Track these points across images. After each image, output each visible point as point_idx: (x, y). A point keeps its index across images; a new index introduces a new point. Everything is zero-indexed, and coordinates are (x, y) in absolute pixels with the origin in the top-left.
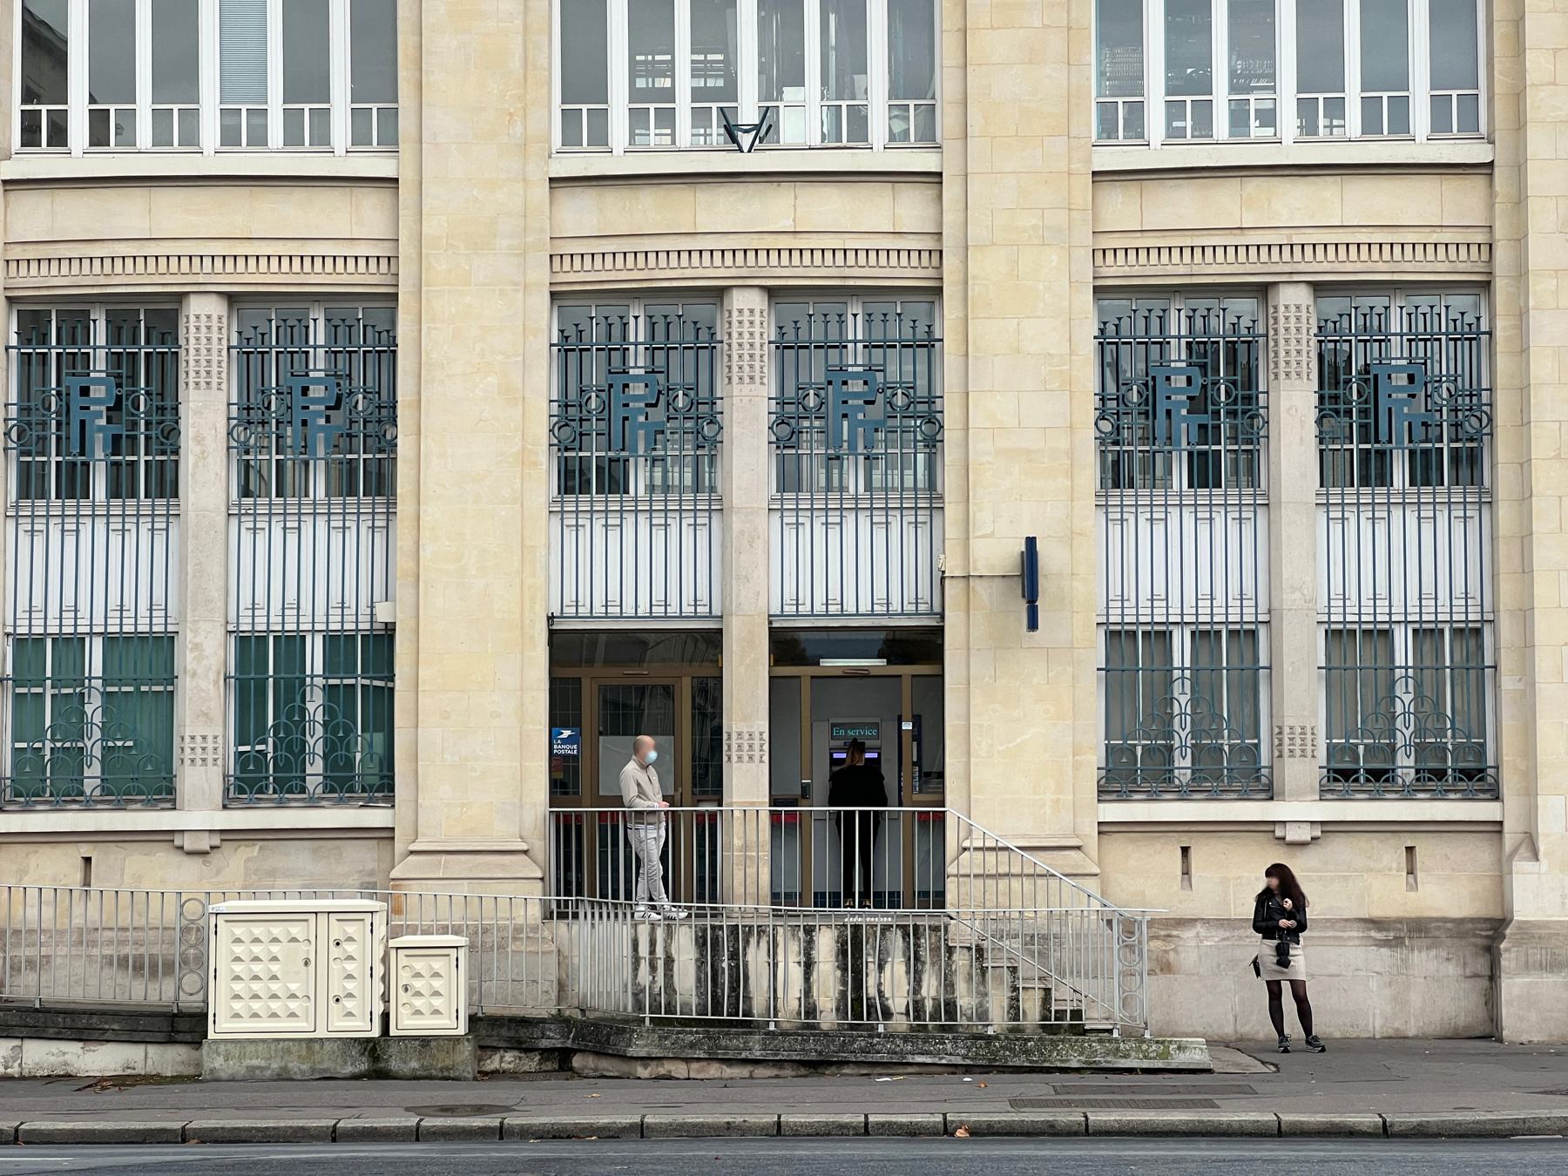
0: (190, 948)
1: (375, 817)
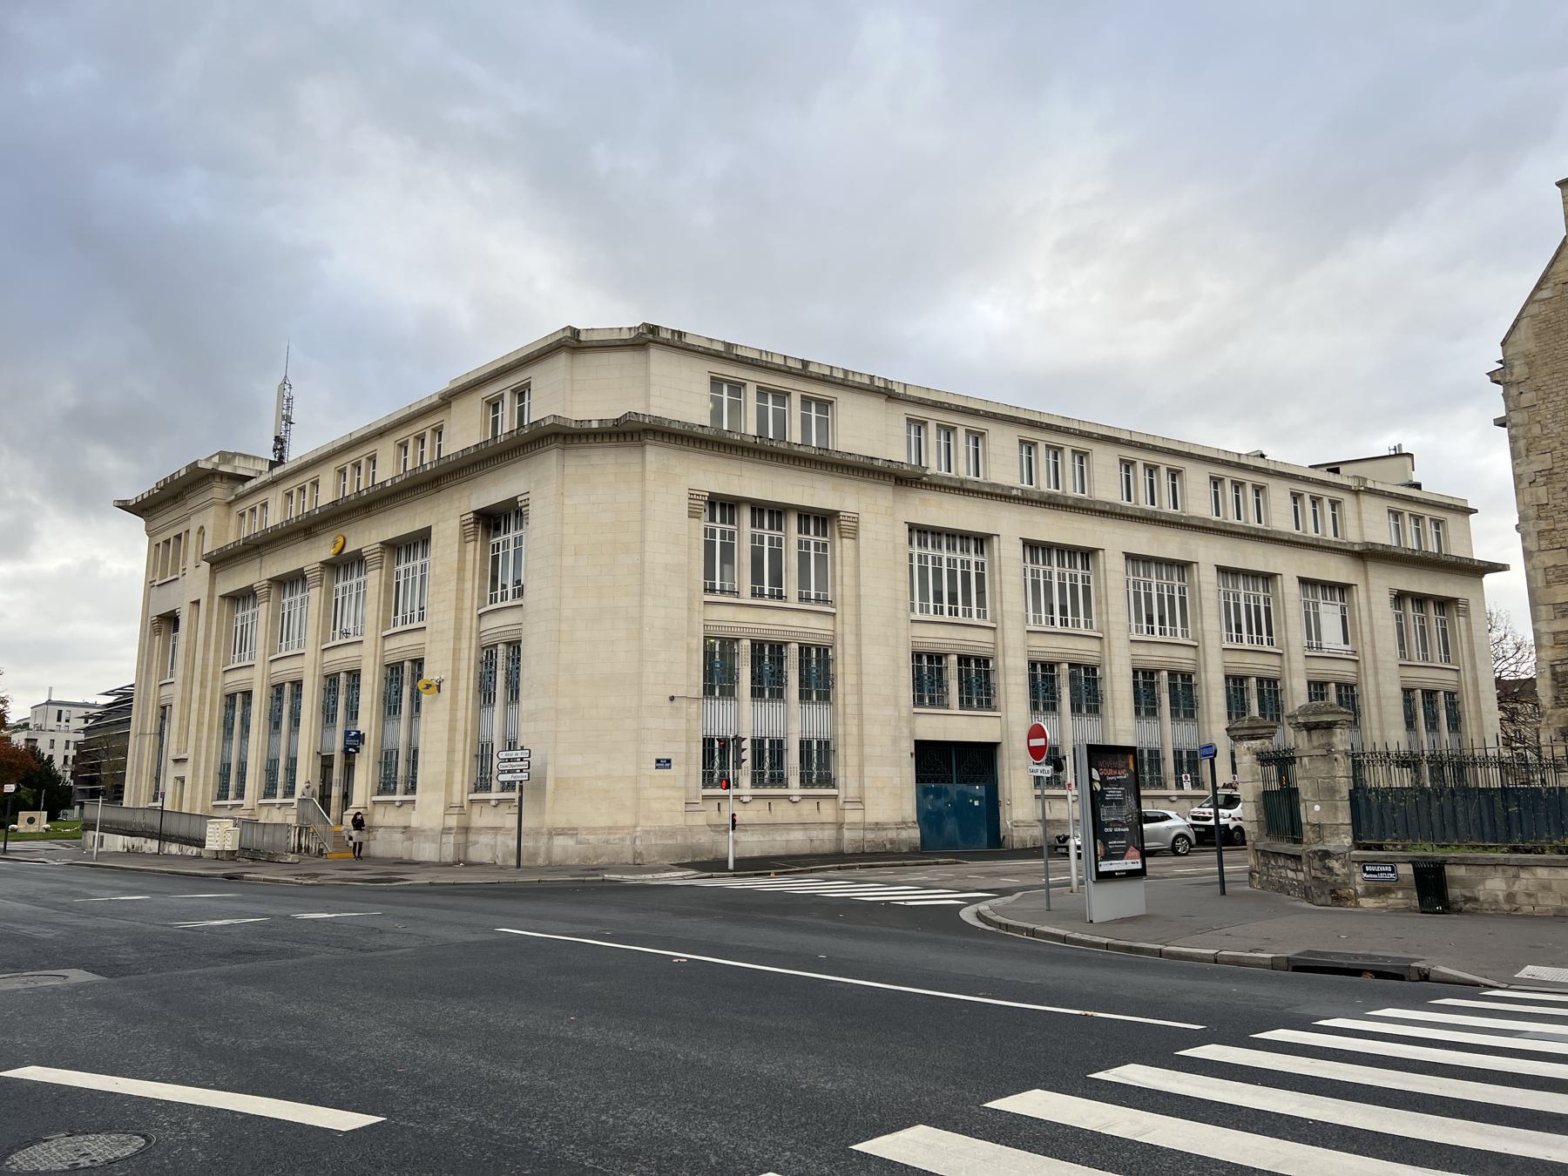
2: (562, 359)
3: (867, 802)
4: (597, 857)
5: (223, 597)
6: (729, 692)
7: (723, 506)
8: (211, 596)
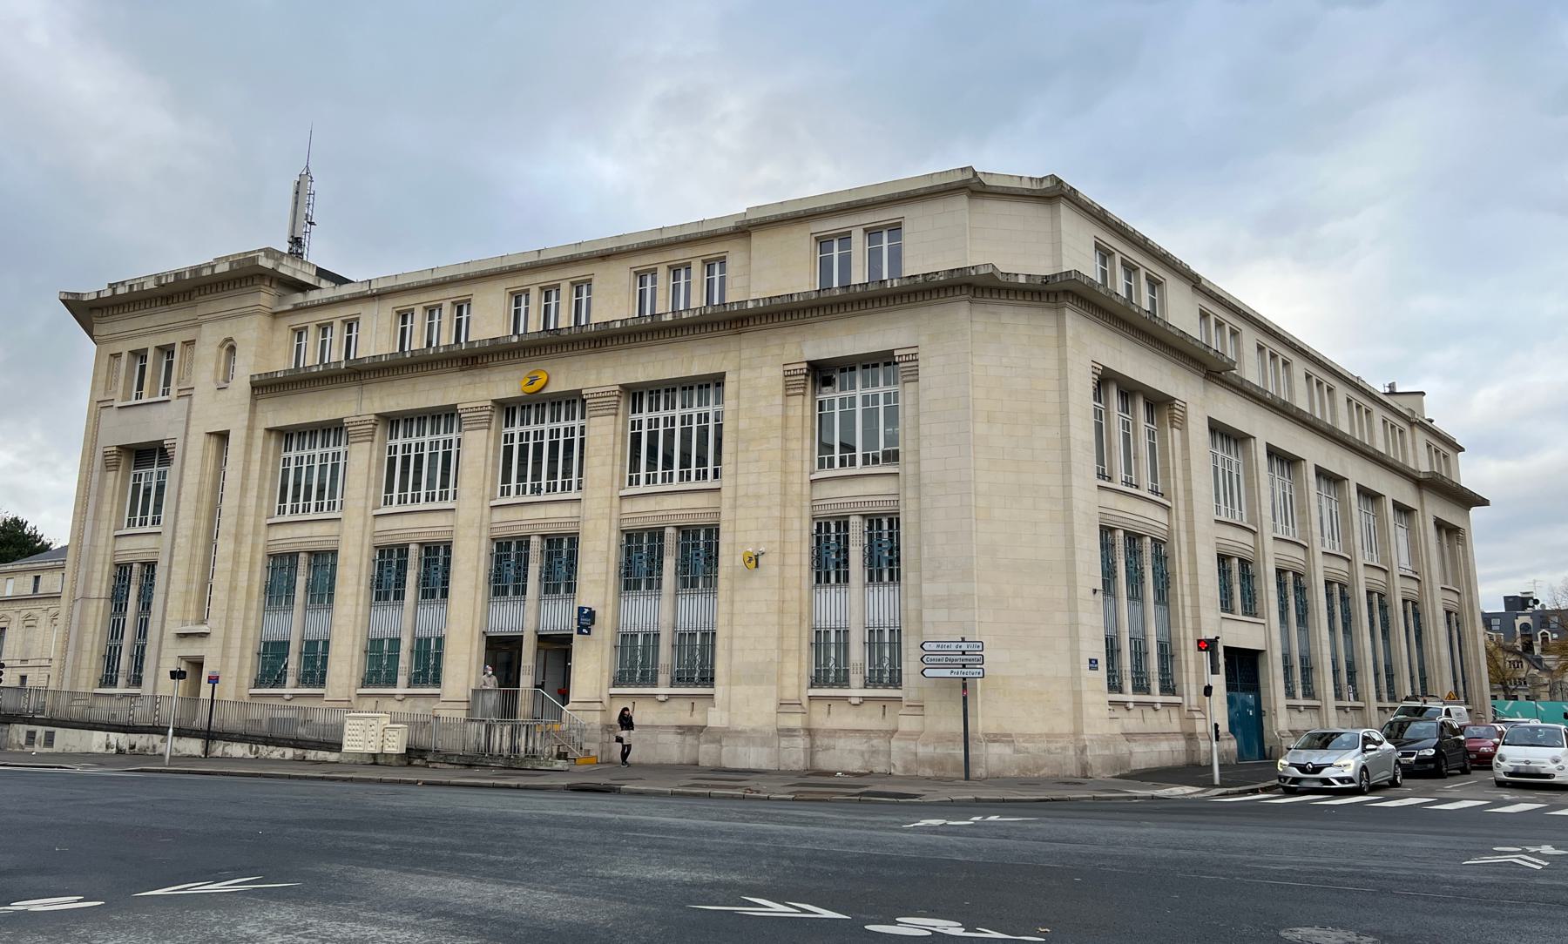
0: (340, 729)
1: (436, 691)
2: (962, 202)
5: (270, 430)
7: (822, 373)
8: (251, 428)
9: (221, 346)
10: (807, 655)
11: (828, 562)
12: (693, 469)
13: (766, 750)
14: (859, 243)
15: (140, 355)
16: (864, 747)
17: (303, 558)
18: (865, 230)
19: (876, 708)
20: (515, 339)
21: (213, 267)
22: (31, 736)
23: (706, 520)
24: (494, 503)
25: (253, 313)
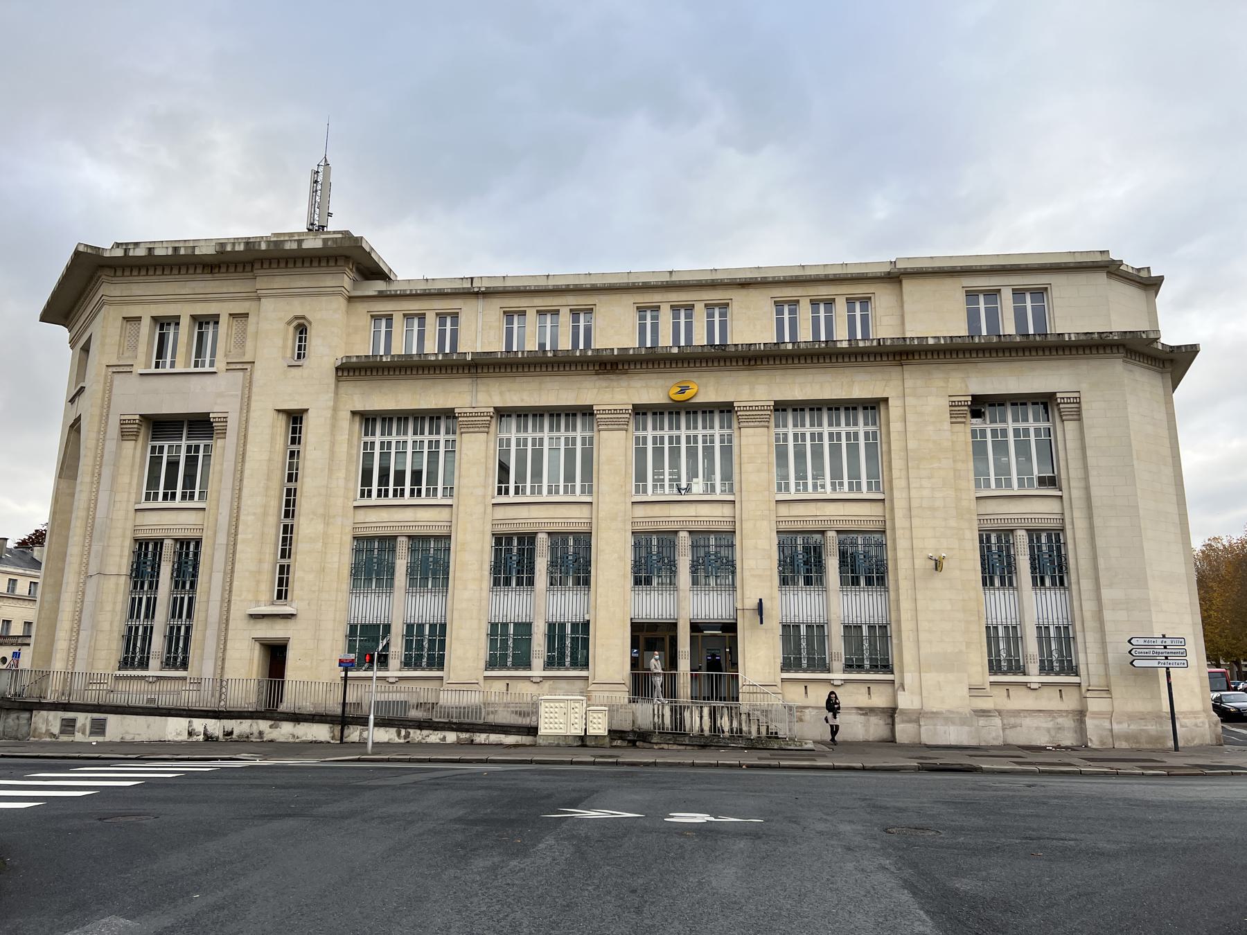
0: (534, 709)
2: (1101, 278)
3: (1113, 689)
4: (1193, 739)
5: (354, 413)
6: (1008, 581)
7: (979, 406)
9: (289, 323)
10: (484, 643)
11: (995, 567)
12: (391, 488)
13: (966, 728)
14: (841, 308)
15: (163, 323)
16: (1050, 725)
17: (402, 546)
18: (672, 306)
19: (1054, 692)
20: (675, 350)
21: (234, 244)
22: (69, 726)
23: (196, 534)
24: (138, 507)
25: (333, 294)
